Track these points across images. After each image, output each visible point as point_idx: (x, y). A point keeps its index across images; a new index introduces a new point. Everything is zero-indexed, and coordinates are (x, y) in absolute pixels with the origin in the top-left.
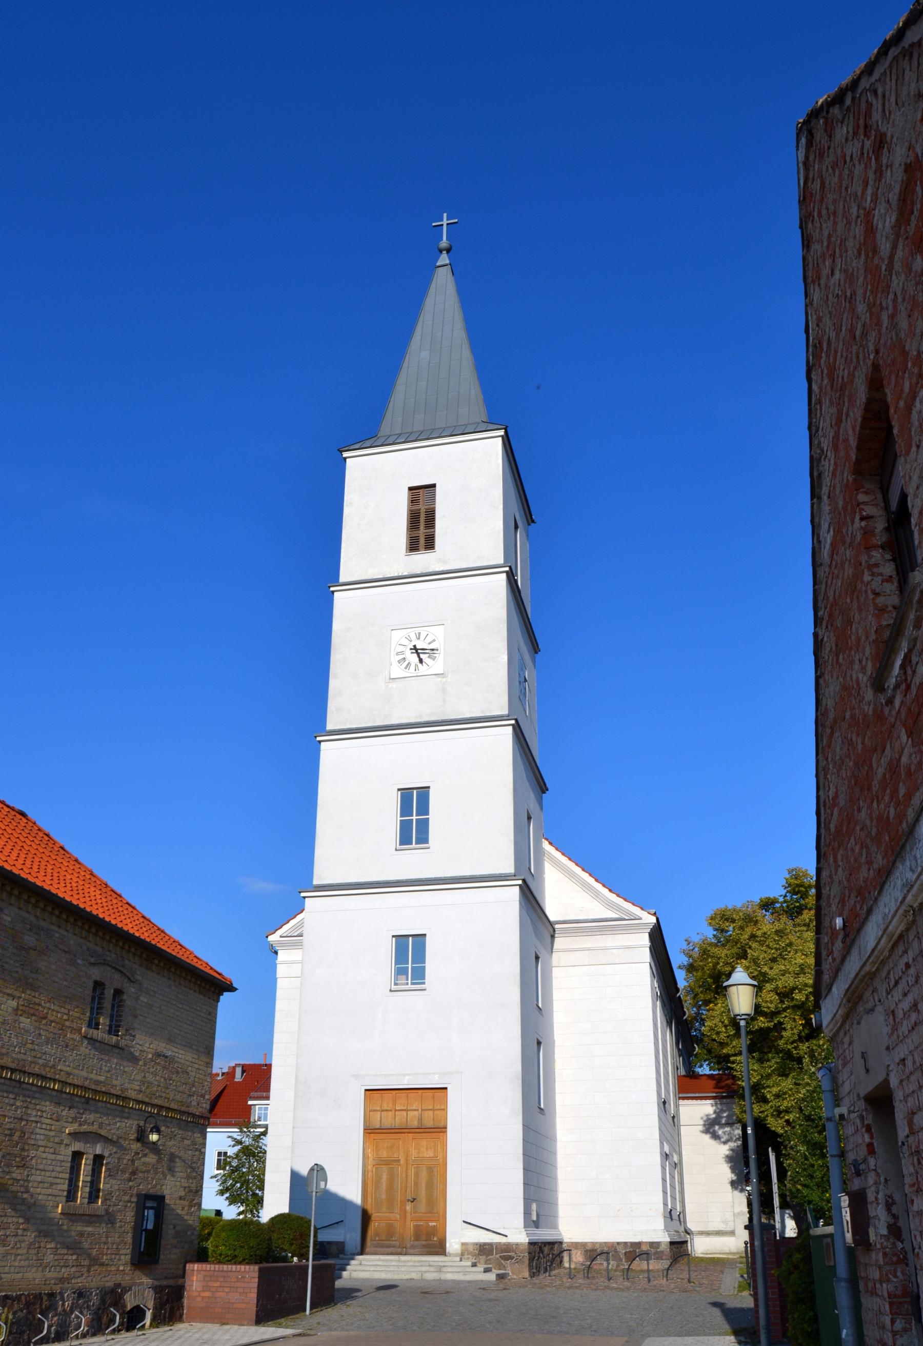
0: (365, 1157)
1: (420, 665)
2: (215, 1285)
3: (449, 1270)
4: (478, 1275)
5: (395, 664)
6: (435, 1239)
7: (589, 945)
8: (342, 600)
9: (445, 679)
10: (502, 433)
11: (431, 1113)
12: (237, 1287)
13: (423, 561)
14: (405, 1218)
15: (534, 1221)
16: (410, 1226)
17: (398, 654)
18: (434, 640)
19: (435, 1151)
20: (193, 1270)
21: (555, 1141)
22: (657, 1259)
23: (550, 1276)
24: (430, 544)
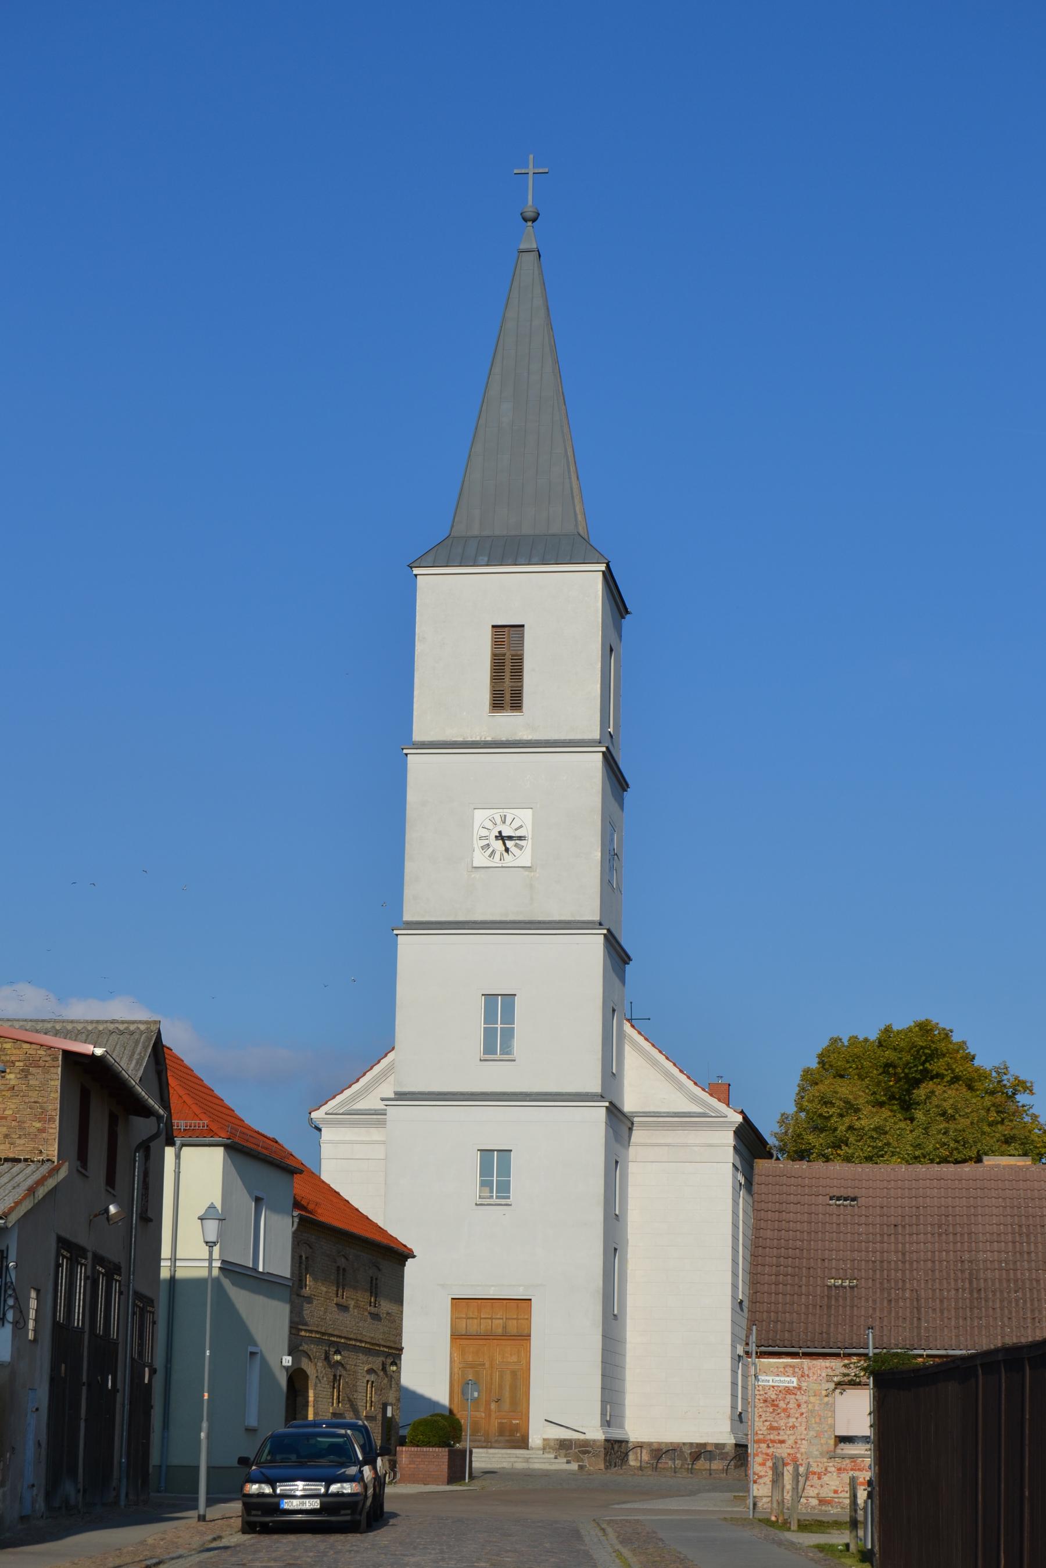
0: (452, 1361)
1: (505, 854)
2: (418, 1460)
3: (536, 1461)
4: (561, 1464)
6: (518, 1435)
7: (669, 1141)
8: (417, 763)
9: (532, 874)
10: (603, 567)
11: (515, 1322)
12: (434, 1462)
14: (490, 1415)
15: (607, 1421)
16: (495, 1423)
17: (481, 838)
18: (521, 827)
19: (518, 1357)
20: (402, 1451)
21: (625, 1342)
22: (722, 1459)
23: (621, 1469)
24: (516, 704)
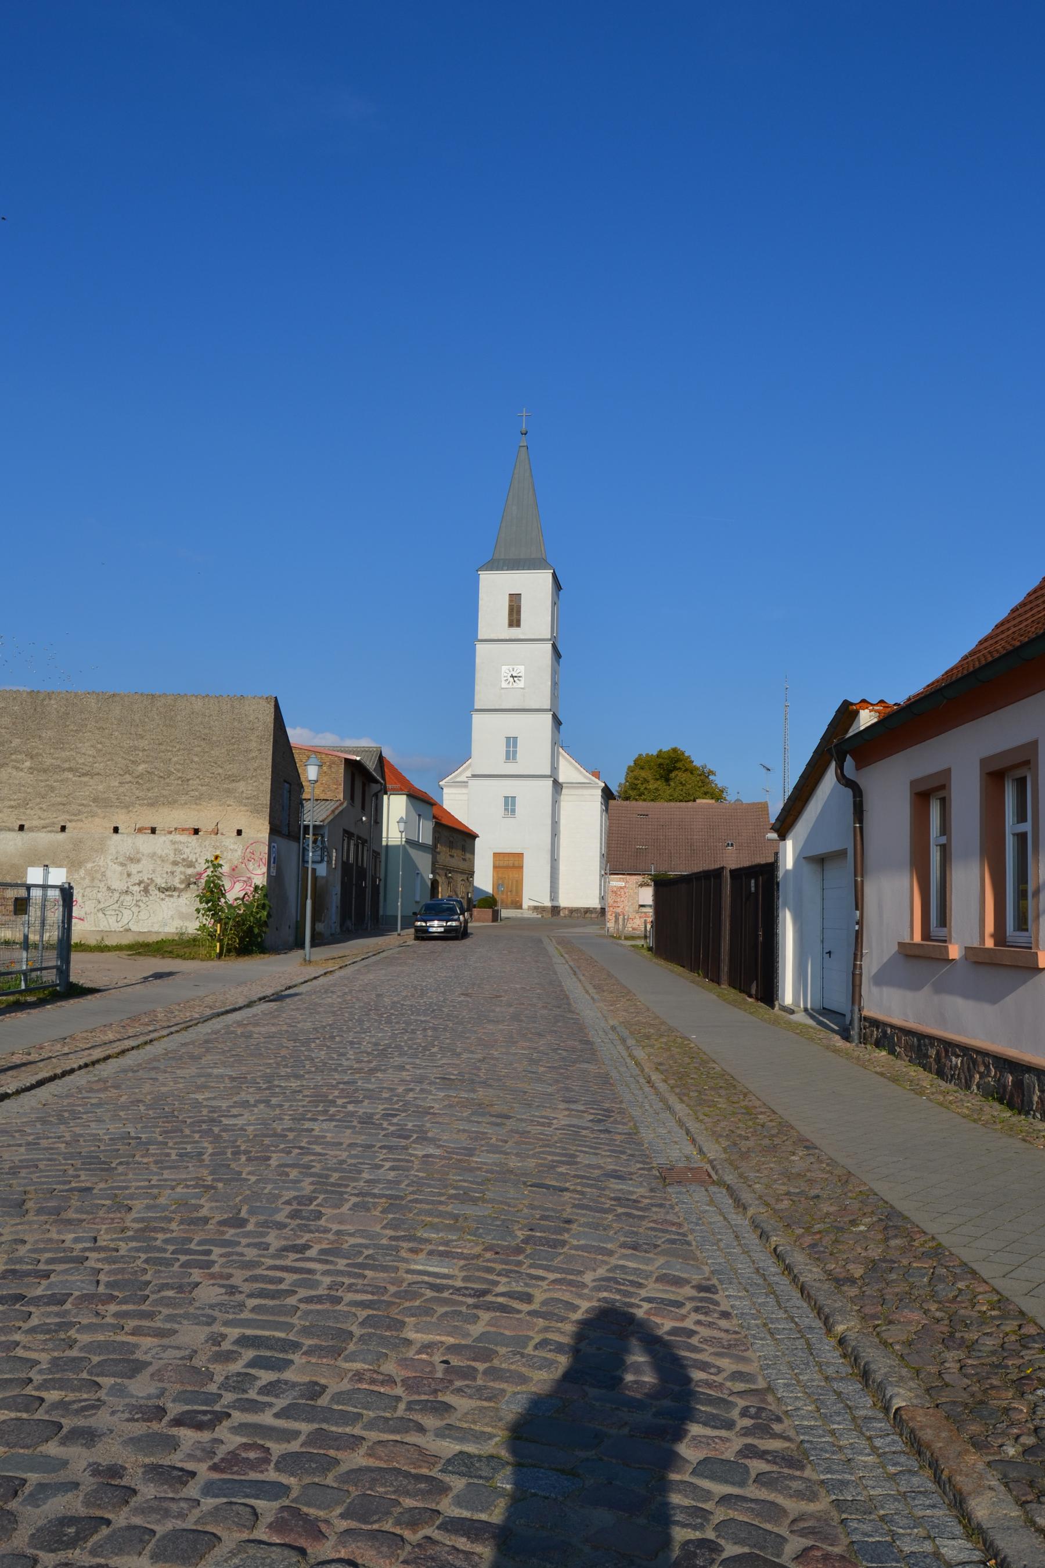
4: (535, 915)
5: (503, 682)
13: (515, 633)
16: (510, 900)
24: (518, 625)
